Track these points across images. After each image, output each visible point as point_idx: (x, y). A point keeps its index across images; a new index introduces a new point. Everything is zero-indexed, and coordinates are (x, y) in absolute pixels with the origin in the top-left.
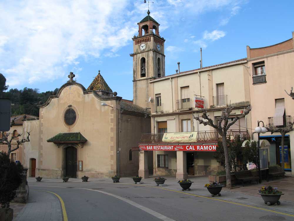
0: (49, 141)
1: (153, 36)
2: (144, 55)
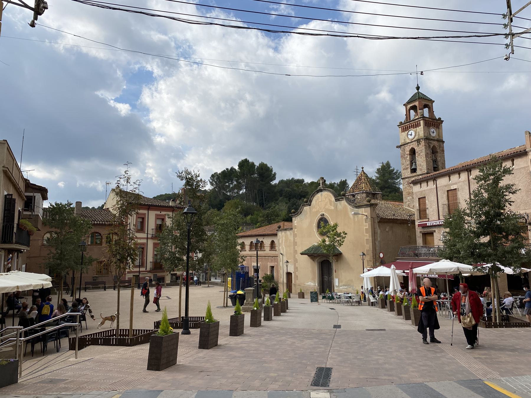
0: (302, 254)
1: (423, 120)
2: (414, 145)
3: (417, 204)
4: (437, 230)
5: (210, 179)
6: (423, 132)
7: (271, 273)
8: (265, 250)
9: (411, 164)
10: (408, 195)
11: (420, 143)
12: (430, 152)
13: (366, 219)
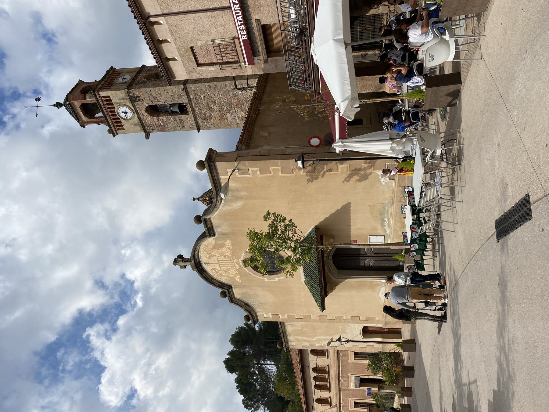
0: (323, 308)
1: (99, 91)
3: (210, 69)
4: (254, 16)
5: (250, 411)
6: (118, 92)
7: (366, 357)
8: (328, 366)
9: (173, 113)
10: (224, 119)
11: (137, 97)
12: (153, 82)
13: (240, 172)
